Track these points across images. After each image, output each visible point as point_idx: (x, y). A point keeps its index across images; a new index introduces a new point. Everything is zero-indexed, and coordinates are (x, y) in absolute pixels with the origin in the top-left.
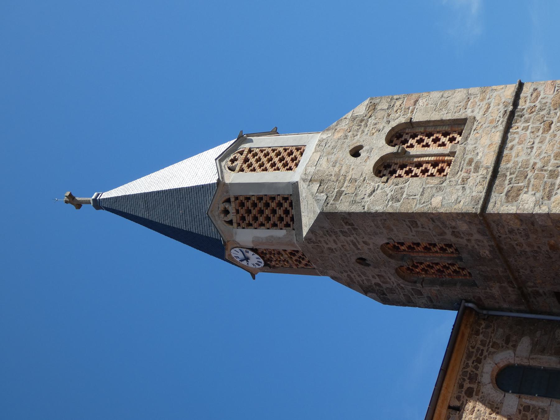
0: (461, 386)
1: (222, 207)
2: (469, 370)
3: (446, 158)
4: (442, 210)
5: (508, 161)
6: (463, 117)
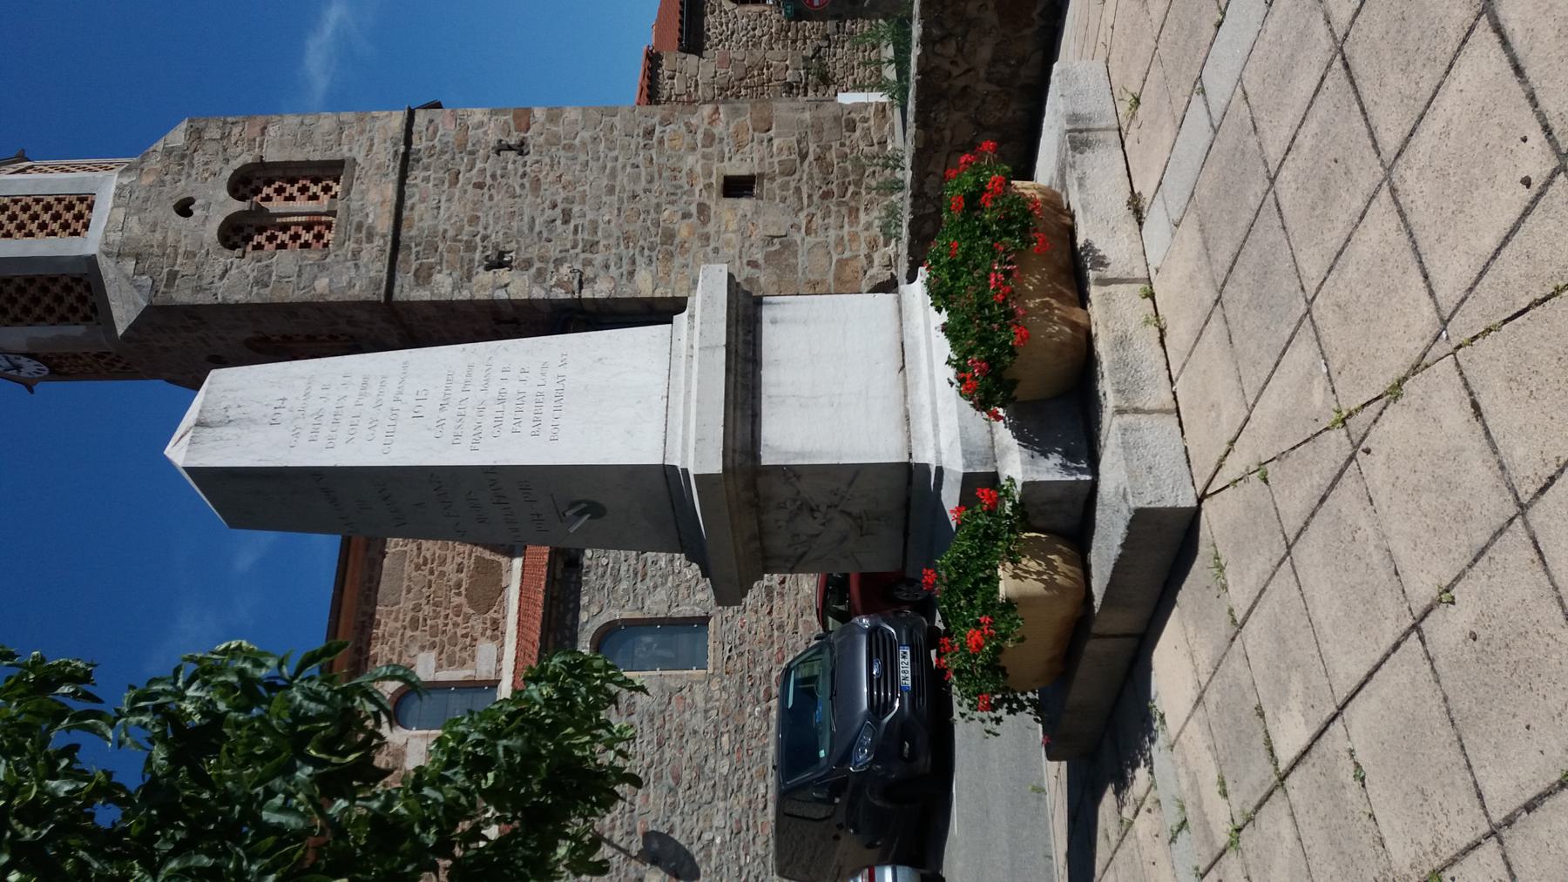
4: (332, 298)
5: (411, 227)
6: (338, 157)
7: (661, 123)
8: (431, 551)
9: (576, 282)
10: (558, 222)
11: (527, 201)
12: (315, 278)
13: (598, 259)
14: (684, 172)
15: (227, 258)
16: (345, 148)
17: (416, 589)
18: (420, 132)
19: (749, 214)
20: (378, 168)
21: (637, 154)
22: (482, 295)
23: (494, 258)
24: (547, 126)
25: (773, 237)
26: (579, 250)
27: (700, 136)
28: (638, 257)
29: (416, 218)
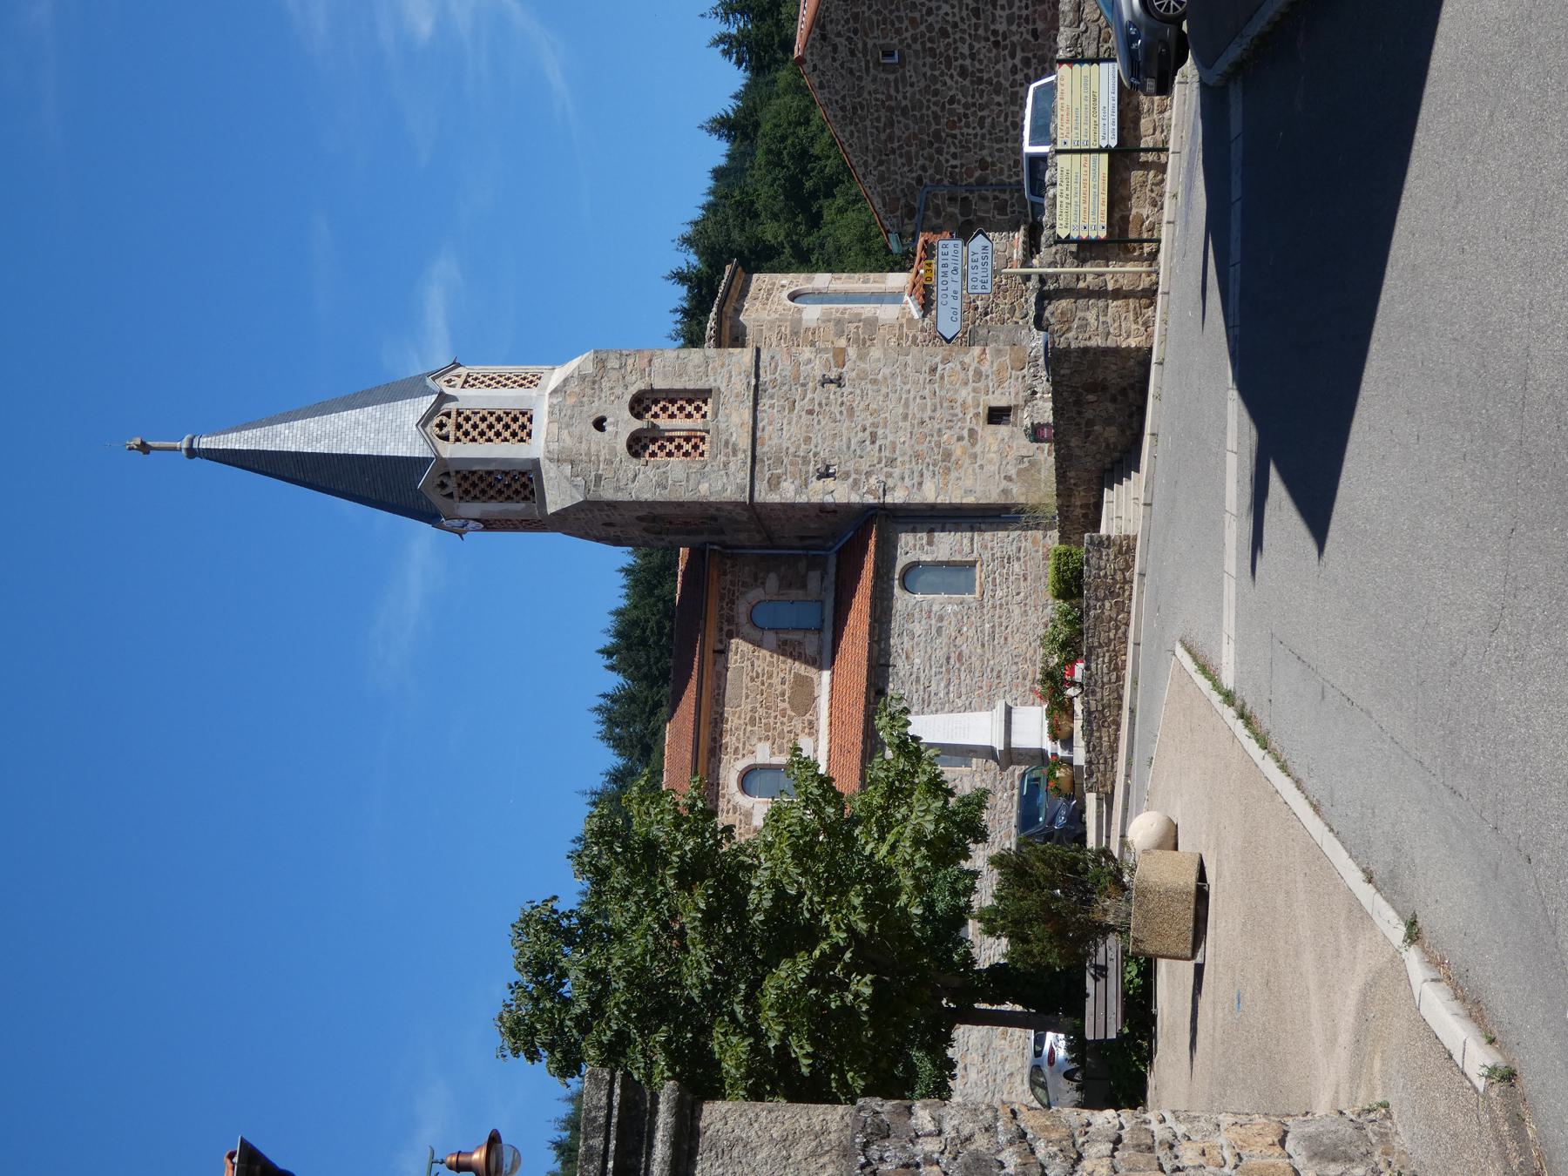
0: (721, 630)
1: (438, 481)
2: (724, 612)
3: (699, 434)
4: (712, 499)
5: (763, 445)
6: (707, 387)
7: (942, 362)
8: (761, 668)
9: (881, 490)
10: (868, 443)
11: (845, 425)
12: (699, 483)
13: (897, 472)
14: (959, 403)
15: (634, 464)
16: (712, 379)
17: (752, 696)
18: (765, 367)
19: (1006, 439)
20: (737, 396)
21: (924, 388)
22: (816, 499)
23: (823, 470)
24: (858, 363)
25: (1023, 457)
26: (883, 465)
27: (971, 373)
28: (925, 471)
29: (767, 437)
